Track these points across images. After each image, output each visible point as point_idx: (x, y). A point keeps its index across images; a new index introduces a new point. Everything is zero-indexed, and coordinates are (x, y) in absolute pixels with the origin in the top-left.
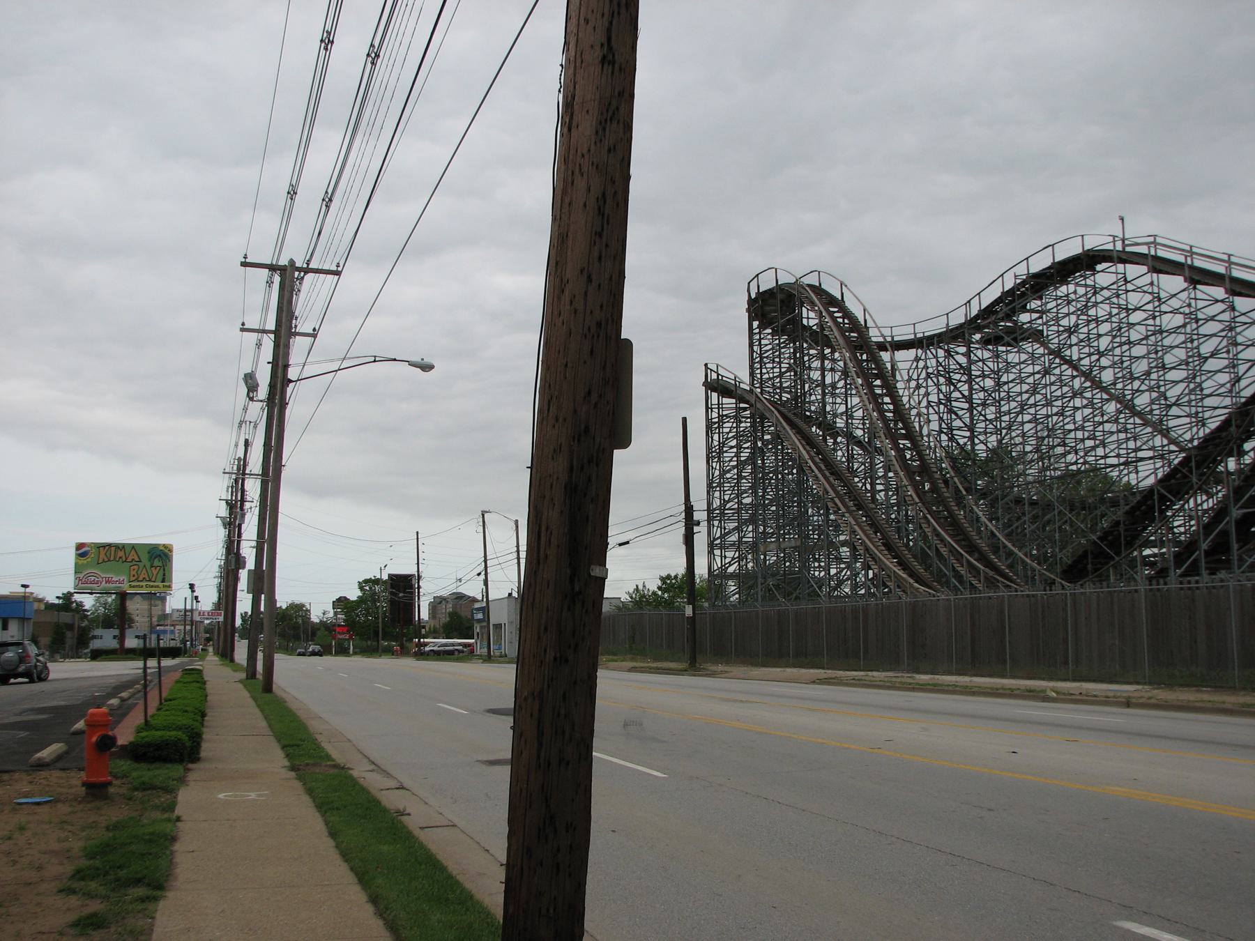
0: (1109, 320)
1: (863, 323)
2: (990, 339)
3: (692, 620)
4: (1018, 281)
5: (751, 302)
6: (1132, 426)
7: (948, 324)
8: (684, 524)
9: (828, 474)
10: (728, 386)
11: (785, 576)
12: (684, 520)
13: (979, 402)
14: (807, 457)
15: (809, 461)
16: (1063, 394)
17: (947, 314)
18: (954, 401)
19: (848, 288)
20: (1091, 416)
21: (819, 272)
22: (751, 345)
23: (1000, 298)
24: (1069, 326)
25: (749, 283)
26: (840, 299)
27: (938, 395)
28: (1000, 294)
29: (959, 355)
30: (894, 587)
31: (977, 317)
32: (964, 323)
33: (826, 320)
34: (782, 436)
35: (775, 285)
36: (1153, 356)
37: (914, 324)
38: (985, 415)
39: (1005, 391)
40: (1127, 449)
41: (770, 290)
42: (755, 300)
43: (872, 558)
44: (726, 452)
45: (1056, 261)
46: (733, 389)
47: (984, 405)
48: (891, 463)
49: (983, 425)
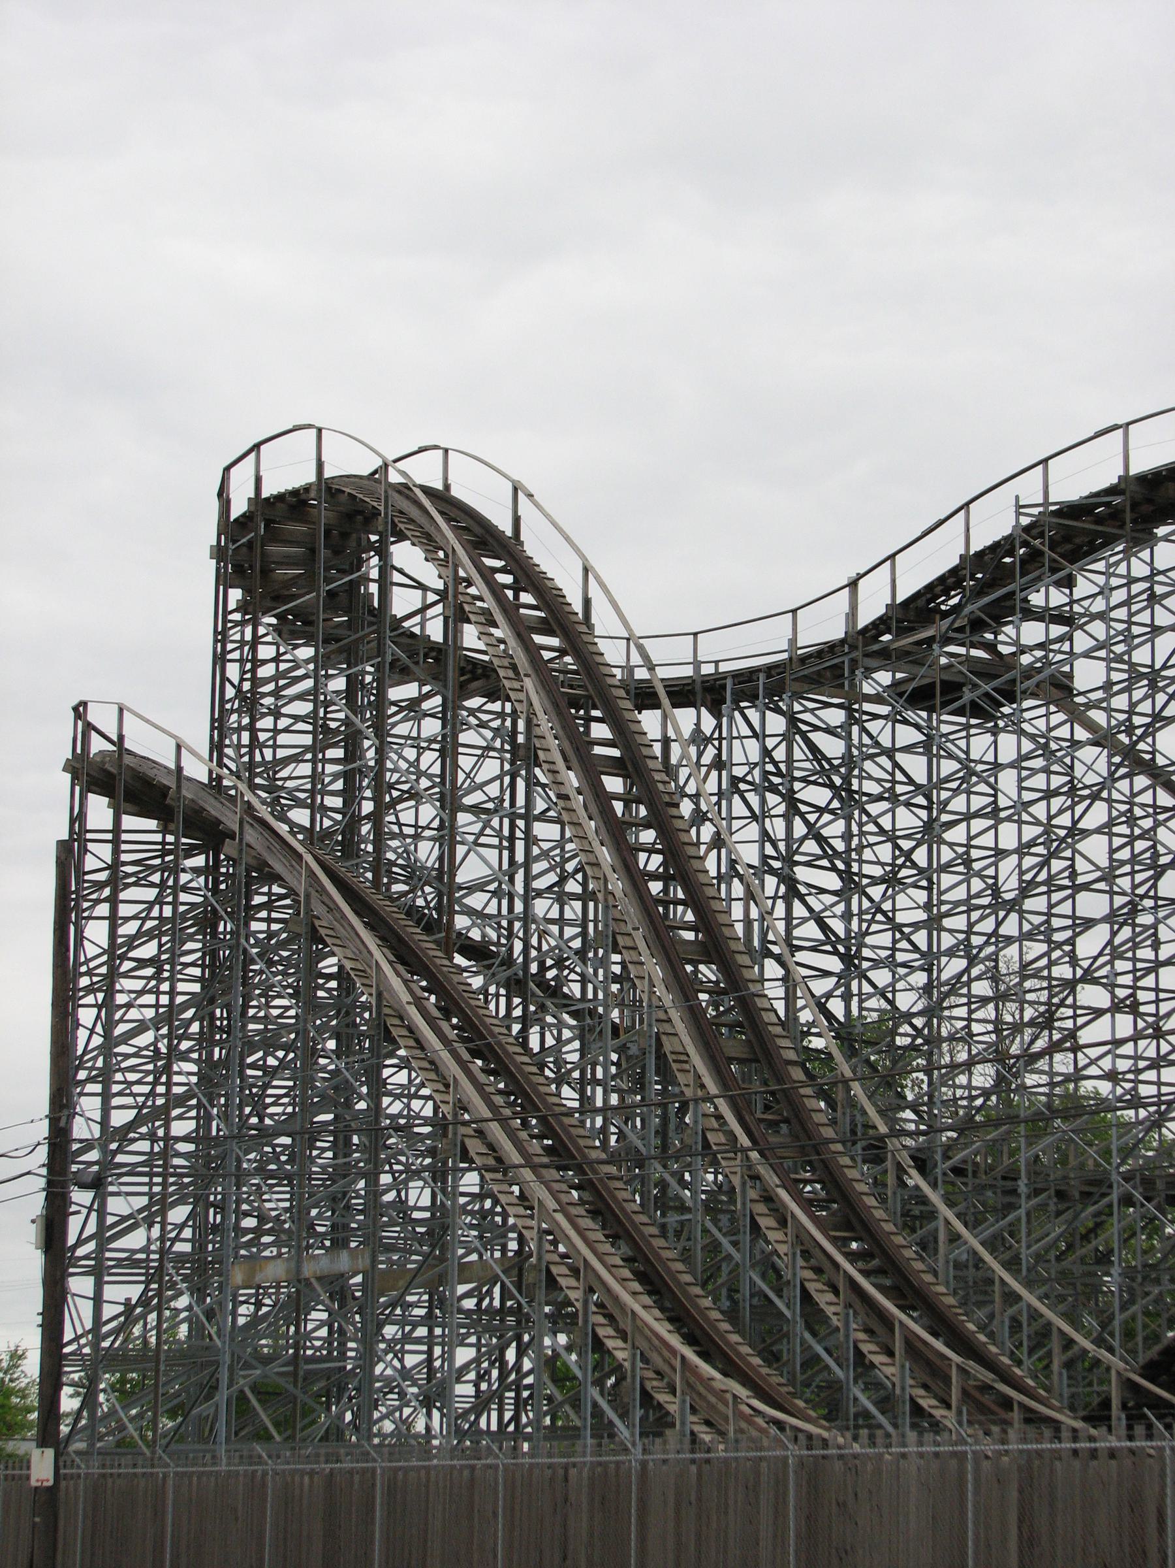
0: (1104, 705)
1: (578, 607)
2: (932, 685)
3: (49, 1497)
4: (1025, 521)
5: (230, 528)
6: (1151, 996)
7: (793, 641)
8: (42, 1182)
9: (466, 1056)
10: (151, 773)
11: (296, 1366)
12: (44, 1171)
13: (877, 871)
14: (405, 997)
15: (413, 1011)
16: (970, 897)
17: (794, 611)
18: (808, 864)
19: (537, 505)
20: (1044, 962)
21: (446, 451)
22: (220, 660)
23: (954, 571)
24: (1152, 666)
25: (227, 469)
26: (509, 533)
27: (762, 848)
28: (956, 561)
29: (820, 733)
30: (682, 1410)
31: (880, 625)
32: (842, 642)
33: (472, 590)
34: (322, 932)
35: (312, 478)
36: (1123, 829)
37: (695, 634)
38: (894, 910)
39: (1038, 823)
40: (1136, 1057)
41: (295, 493)
42: (245, 521)
43: (605, 1316)
44: (126, 975)
45: (1134, 470)
46: (170, 782)
47: (891, 880)
48: (667, 1028)
49: (885, 939)
